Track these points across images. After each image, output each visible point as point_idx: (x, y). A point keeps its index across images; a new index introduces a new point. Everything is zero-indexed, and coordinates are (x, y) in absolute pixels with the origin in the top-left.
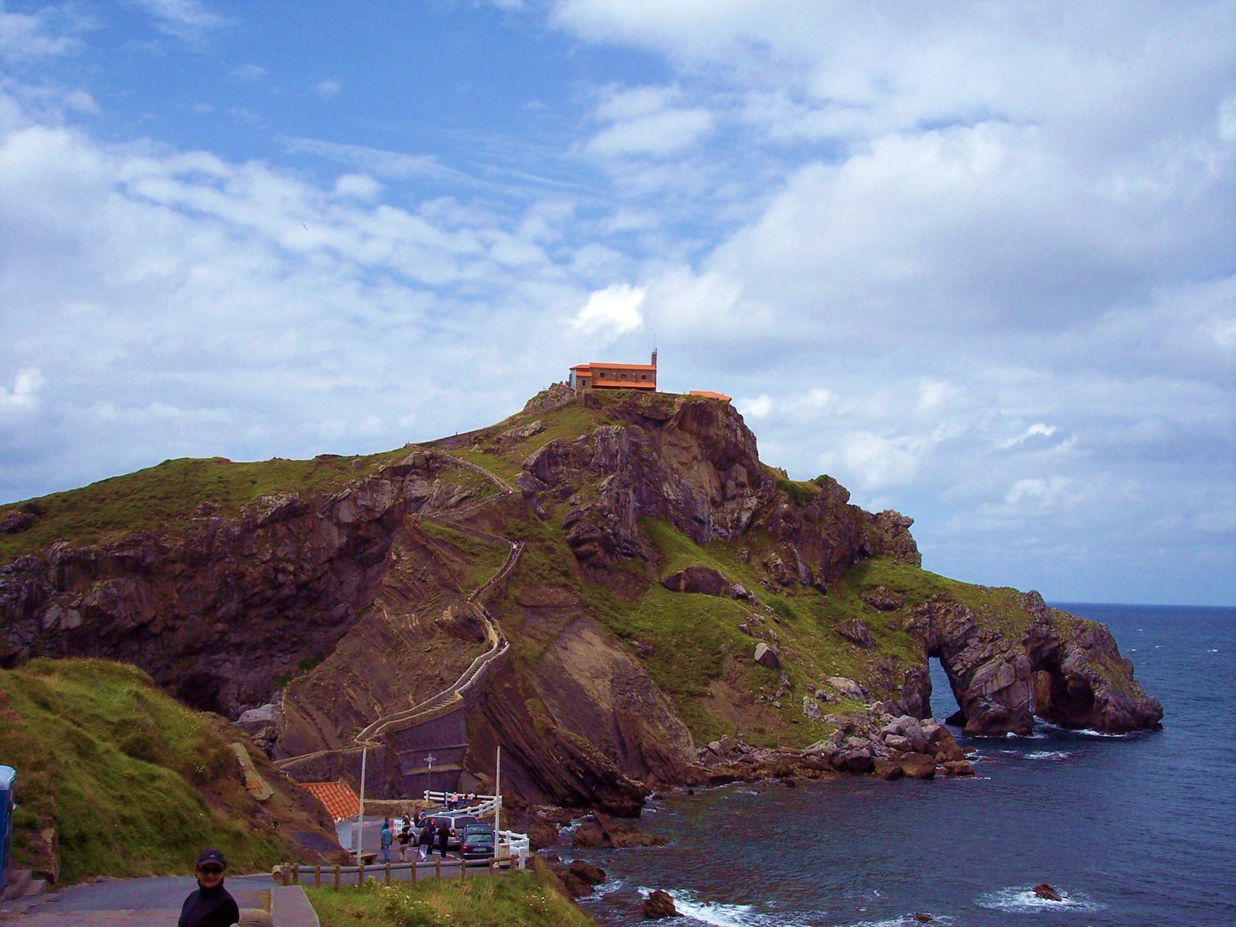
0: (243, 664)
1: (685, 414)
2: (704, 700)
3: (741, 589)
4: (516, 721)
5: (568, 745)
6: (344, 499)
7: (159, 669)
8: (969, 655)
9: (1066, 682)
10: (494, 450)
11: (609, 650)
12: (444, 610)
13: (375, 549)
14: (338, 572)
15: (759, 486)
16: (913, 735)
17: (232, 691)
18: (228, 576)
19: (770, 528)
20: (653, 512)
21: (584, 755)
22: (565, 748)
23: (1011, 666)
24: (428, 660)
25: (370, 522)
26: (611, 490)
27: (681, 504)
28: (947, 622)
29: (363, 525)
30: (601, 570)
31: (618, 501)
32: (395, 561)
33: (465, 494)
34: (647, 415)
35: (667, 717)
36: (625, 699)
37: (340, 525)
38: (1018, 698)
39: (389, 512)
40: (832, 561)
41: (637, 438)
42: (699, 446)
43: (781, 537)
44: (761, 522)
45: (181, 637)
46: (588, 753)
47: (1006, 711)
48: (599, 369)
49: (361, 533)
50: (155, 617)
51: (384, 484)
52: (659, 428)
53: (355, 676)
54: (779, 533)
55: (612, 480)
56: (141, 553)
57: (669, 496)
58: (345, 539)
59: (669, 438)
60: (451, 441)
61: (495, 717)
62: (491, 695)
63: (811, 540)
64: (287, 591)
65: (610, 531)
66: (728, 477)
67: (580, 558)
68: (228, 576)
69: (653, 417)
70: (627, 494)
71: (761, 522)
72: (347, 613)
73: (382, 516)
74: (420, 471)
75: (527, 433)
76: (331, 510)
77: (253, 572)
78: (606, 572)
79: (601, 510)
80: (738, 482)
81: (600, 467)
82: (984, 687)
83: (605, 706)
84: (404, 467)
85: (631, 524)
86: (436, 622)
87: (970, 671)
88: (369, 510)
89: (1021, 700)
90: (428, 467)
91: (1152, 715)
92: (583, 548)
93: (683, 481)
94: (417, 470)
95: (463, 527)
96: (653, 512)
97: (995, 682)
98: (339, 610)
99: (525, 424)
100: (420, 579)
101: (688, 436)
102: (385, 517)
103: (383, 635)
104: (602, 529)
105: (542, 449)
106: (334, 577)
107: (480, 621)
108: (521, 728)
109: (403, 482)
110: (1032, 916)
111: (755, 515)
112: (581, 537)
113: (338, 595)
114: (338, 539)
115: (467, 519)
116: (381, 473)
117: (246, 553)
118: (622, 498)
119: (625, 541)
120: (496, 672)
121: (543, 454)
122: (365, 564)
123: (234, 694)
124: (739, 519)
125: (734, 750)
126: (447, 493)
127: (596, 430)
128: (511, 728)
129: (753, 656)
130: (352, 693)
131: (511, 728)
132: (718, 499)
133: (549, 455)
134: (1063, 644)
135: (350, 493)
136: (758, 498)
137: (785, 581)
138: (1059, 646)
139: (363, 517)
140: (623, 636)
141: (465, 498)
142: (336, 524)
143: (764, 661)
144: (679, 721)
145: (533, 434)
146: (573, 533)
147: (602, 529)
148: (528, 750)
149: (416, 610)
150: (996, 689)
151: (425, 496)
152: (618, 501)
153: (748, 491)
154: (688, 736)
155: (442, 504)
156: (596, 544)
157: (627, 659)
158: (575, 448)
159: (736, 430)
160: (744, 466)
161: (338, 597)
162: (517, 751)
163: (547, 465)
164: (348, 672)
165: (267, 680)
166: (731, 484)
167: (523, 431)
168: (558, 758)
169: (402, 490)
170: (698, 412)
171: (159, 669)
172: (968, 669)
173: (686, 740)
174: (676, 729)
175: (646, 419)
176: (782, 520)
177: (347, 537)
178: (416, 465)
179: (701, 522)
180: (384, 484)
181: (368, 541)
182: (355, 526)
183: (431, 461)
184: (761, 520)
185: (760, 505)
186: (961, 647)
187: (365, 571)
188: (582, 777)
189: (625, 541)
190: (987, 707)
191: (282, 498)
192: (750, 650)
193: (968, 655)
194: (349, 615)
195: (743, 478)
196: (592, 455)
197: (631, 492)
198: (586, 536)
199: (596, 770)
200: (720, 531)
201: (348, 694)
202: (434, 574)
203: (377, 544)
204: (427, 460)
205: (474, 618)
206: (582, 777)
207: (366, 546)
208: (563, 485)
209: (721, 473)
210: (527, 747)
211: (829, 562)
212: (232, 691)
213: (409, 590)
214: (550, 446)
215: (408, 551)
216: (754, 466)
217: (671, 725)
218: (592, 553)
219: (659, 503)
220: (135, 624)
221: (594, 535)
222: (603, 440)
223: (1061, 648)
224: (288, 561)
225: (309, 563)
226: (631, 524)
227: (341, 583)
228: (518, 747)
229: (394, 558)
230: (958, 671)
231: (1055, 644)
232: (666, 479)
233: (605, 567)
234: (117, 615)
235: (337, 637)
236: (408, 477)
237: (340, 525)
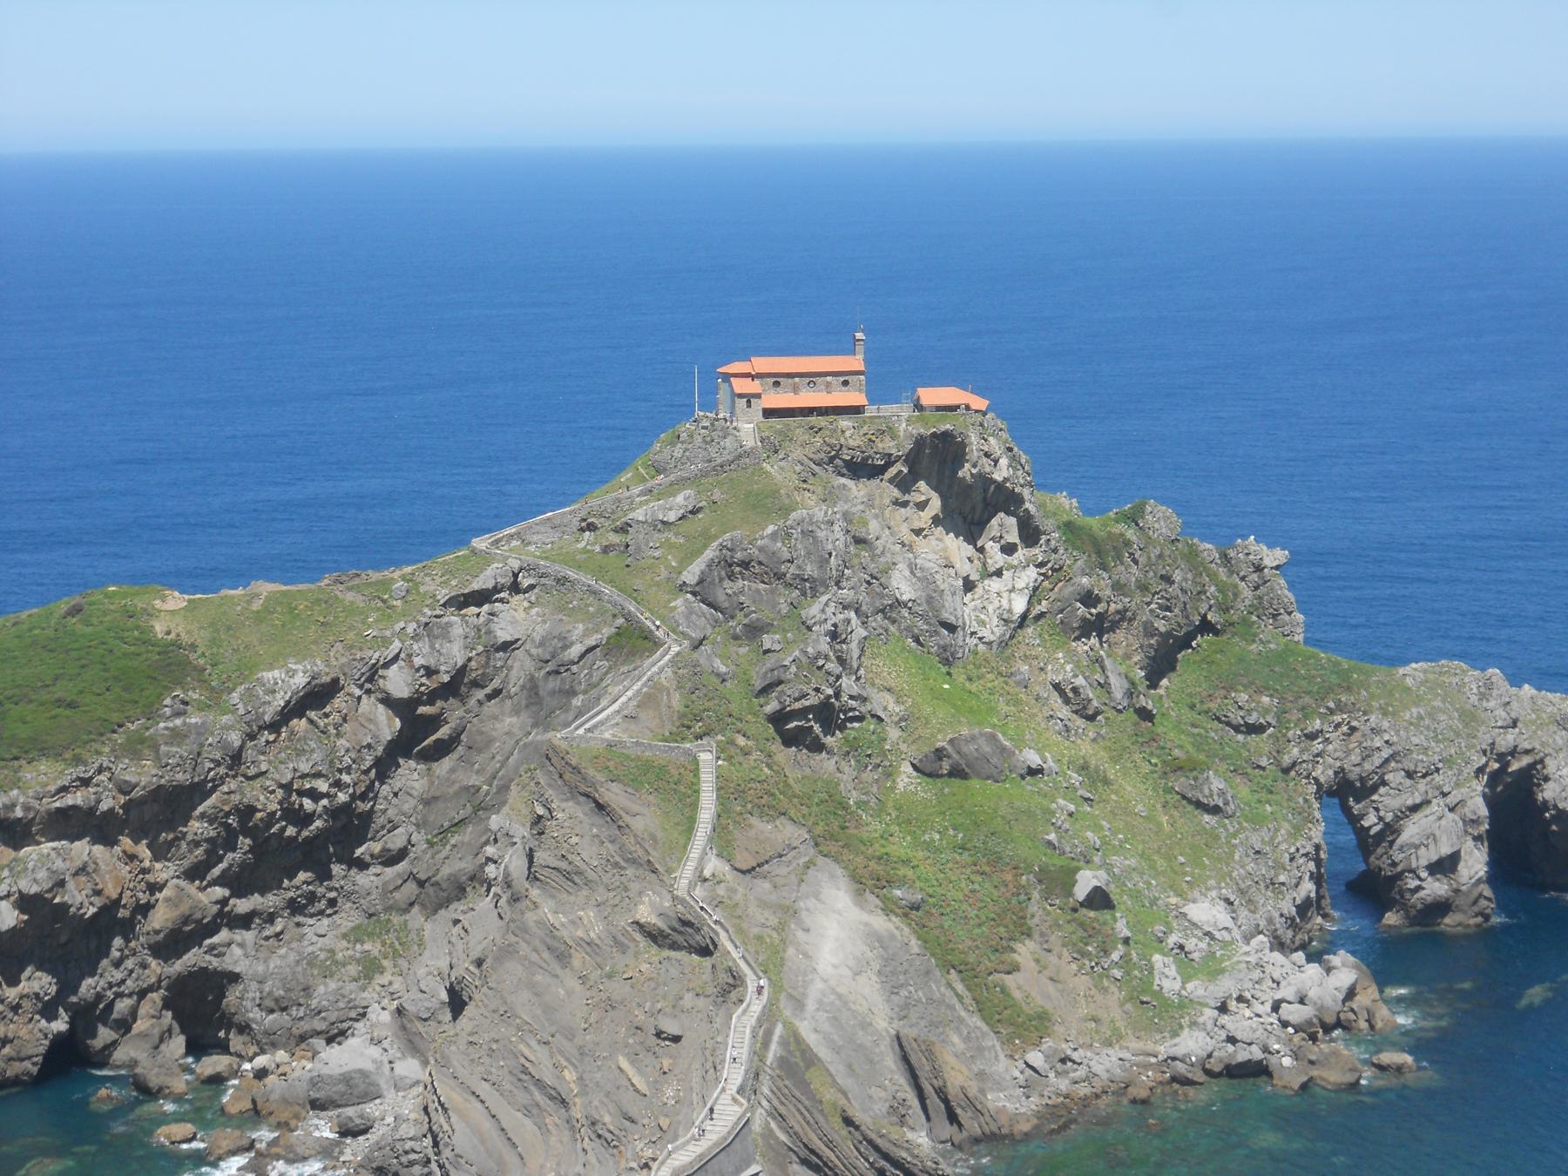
0: (258, 947)
7: (131, 971)
8: (1389, 801)
9: (1548, 823)
16: (1319, 1002)
17: (251, 995)
18: (228, 814)
23: (1457, 818)
28: (1352, 746)
37: (388, 701)
38: (1470, 868)
45: (161, 919)
47: (1450, 893)
50: (121, 894)
51: (449, 624)
56: (93, 796)
64: (318, 823)
68: (228, 814)
72: (409, 841)
76: (370, 680)
77: (268, 802)
82: (1413, 857)
87: (1391, 830)
88: (430, 672)
89: (1473, 872)
97: (1432, 847)
108: (812, 1121)
110: (1466, 936)
112: (788, 709)
114: (387, 726)
117: (251, 772)
123: (254, 999)
128: (798, 1122)
129: (1070, 894)
131: (798, 1122)
134: (1541, 761)
137: (1090, 712)
138: (1535, 763)
146: (772, 706)
147: (817, 690)
150: (1435, 858)
151: (519, 639)
155: (553, 657)
157: (891, 926)
158: (761, 549)
163: (717, 580)
165: (299, 969)
171: (131, 971)
172: (1387, 825)
176: (1079, 604)
179: (952, 628)
180: (449, 624)
186: (1374, 789)
190: (1419, 888)
191: (295, 671)
193: (1387, 800)
198: (797, 705)
208: (746, 616)
212: (251, 995)
213: (579, 873)
220: (95, 910)
221: (807, 703)
223: (1539, 767)
224: (318, 775)
225: (349, 773)
228: (812, 1151)
230: (1370, 827)
231: (1526, 761)
234: (70, 902)
235: (400, 882)
237: (388, 701)
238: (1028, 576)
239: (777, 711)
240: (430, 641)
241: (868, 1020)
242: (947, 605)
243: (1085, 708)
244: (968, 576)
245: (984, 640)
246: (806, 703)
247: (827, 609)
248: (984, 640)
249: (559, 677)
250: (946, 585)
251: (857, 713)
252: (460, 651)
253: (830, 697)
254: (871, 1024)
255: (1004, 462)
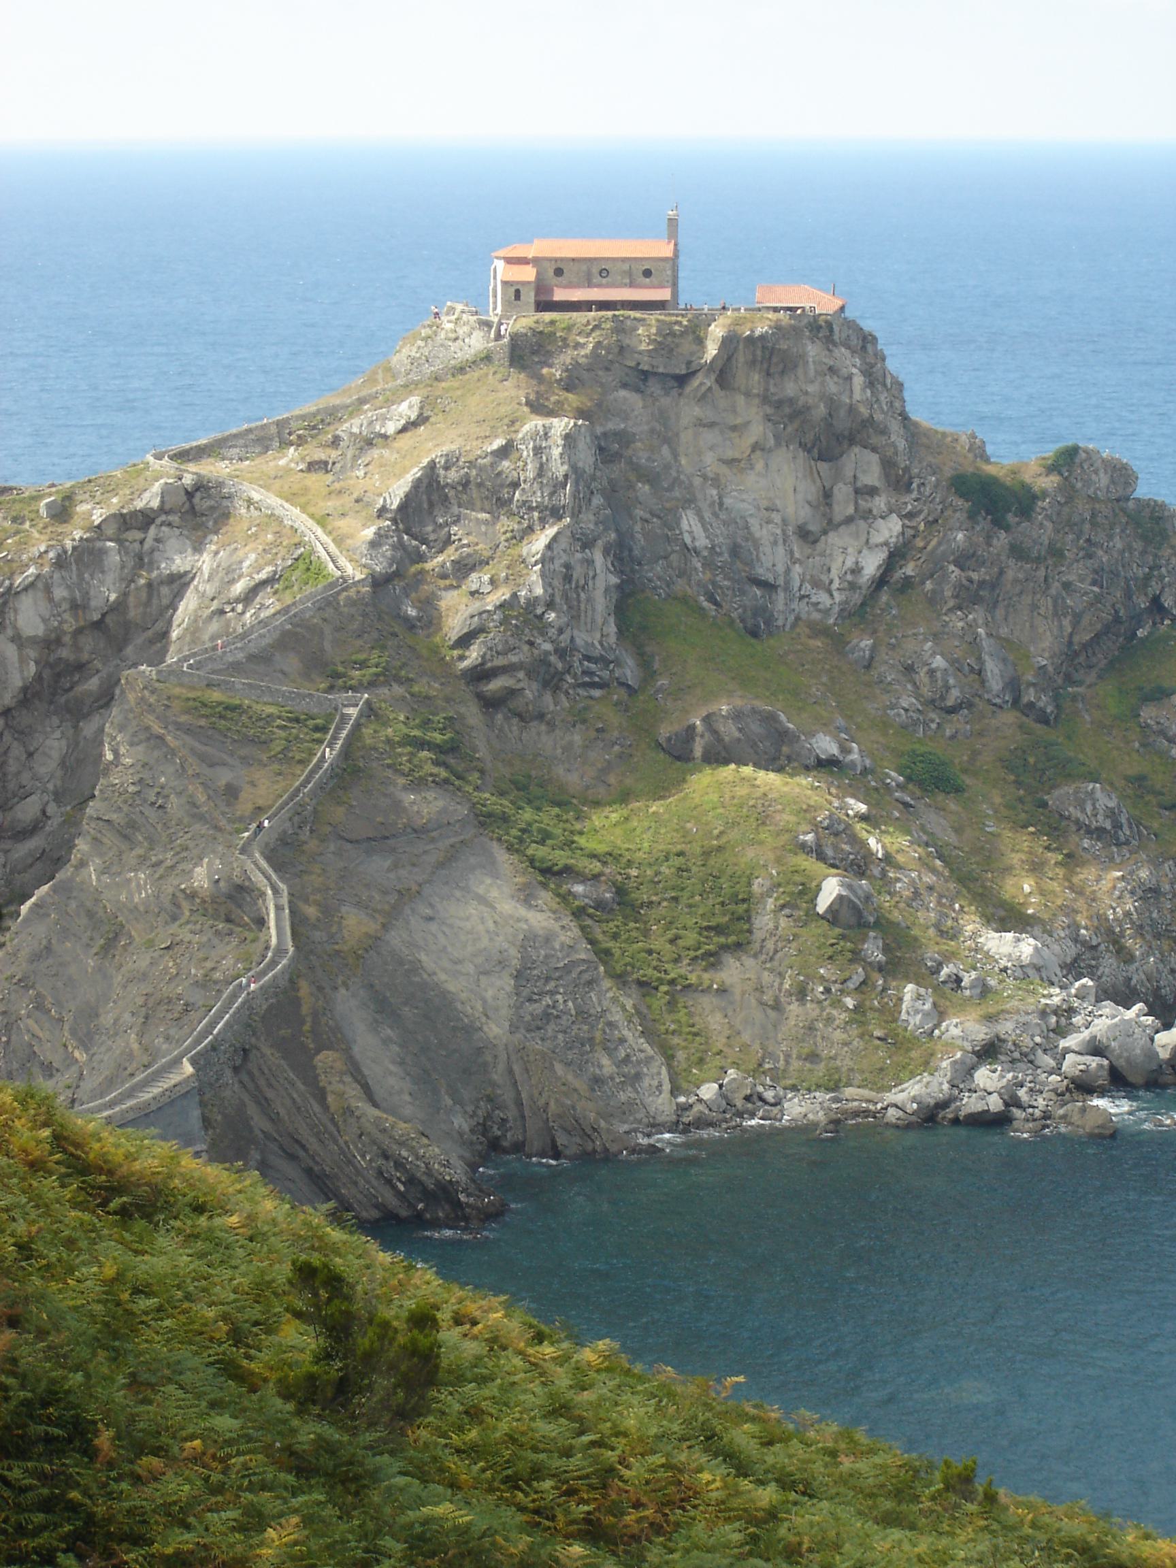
1: (729, 359)
2: (706, 1001)
3: (826, 745)
4: (295, 1096)
5: (380, 1136)
6: (26, 589)
10: (326, 463)
11: (522, 911)
12: (196, 865)
13: (93, 684)
14: (22, 733)
15: (908, 489)
19: (929, 585)
20: (659, 578)
21: (404, 1153)
22: (374, 1142)
24: (166, 968)
25: (79, 631)
26: (552, 559)
27: (720, 554)
29: (67, 639)
30: (535, 723)
31: (568, 578)
32: (112, 763)
33: (263, 575)
34: (646, 368)
35: (622, 1040)
36: (539, 1011)
39: (119, 607)
40: (1076, 639)
41: (626, 418)
42: (768, 418)
43: (951, 603)
44: (910, 569)
46: (412, 1150)
48: (549, 260)
49: (64, 653)
52: (674, 392)
53: (38, 995)
54: (948, 593)
55: (555, 539)
57: (694, 539)
58: (32, 668)
59: (697, 411)
60: (241, 442)
61: (257, 1087)
62: (254, 1051)
63: (1027, 600)
65: (547, 647)
66: (837, 476)
67: (490, 704)
69: (661, 370)
70: (590, 562)
71: (910, 569)
72: (44, 812)
73: (104, 615)
74: (174, 518)
75: (391, 428)
78: (543, 727)
79: (532, 602)
80: (859, 484)
81: (531, 509)
83: (496, 1030)
84: (144, 513)
85: (600, 621)
86: (183, 891)
90: (193, 507)
91: (82, 1505)
92: (495, 685)
93: (728, 501)
94: (170, 518)
95: (239, 681)
96: (659, 578)
98: (27, 811)
99: (389, 402)
100: (153, 804)
101: (741, 400)
102: (108, 620)
103: (90, 914)
104: (531, 644)
105: (415, 473)
106: (15, 744)
107: (259, 890)
109: (142, 542)
111: (896, 556)
112: (489, 665)
113: (25, 778)
115: (251, 658)
116: (99, 527)
118: (578, 573)
119: (588, 658)
120: (264, 1007)
121: (417, 484)
122: (77, 713)
124: (857, 570)
125: (748, 1098)
126: (229, 571)
127: (526, 428)
129: (813, 902)
130: (35, 1028)
132: (813, 527)
133: (430, 485)
135: (38, 576)
136: (901, 517)
139: (66, 622)
140: (548, 872)
141: (264, 583)
142: (12, 640)
143: (833, 917)
144: (646, 1046)
145: (403, 430)
147: (531, 644)
148: (313, 1144)
149: (148, 863)
151: (186, 573)
152: (568, 578)
153: (880, 503)
154: (659, 1074)
156: (521, 675)
158: (481, 469)
159: (849, 378)
160: (874, 450)
161: (24, 783)
162: (297, 1146)
163: (425, 506)
164: (27, 988)
166: (842, 492)
167: (384, 419)
168: (363, 1157)
169: (141, 559)
170: (759, 353)
173: (655, 1083)
174: (639, 1062)
175: (645, 375)
176: (952, 568)
177: (37, 663)
178: (167, 507)
179: (768, 587)
181: (80, 667)
182: (50, 642)
183: (198, 495)
184: (911, 565)
185: (910, 532)
187: (76, 727)
188: (402, 1188)
189: (588, 658)
192: (809, 892)
194: (49, 818)
195: (872, 476)
196: (515, 485)
197: (598, 557)
198: (500, 661)
199: (424, 1178)
200: (814, 599)
201: (29, 1031)
202: (179, 794)
203: (98, 671)
204: (189, 494)
205: (247, 884)
206: (402, 1188)
207: (76, 678)
209: (823, 466)
210: (313, 1140)
211: (1070, 643)
213: (132, 825)
214: (432, 465)
215: (132, 744)
216: (895, 447)
217: (628, 1056)
218: (512, 693)
219: (674, 557)
222: (538, 451)
226: (600, 621)
227: (30, 755)
229: (109, 756)
232: (689, 501)
233: (541, 716)
236: (152, 531)
238: (890, 530)
239: (476, 667)
240: (78, 569)
241: (478, 1024)
242: (763, 558)
243: (943, 698)
244: (805, 524)
245: (820, 606)
246: (513, 659)
247: (555, 545)
248: (820, 606)
249: (223, 618)
250: (764, 531)
251: (597, 679)
252: (114, 584)
253: (547, 653)
254: (481, 1029)
255: (858, 380)
